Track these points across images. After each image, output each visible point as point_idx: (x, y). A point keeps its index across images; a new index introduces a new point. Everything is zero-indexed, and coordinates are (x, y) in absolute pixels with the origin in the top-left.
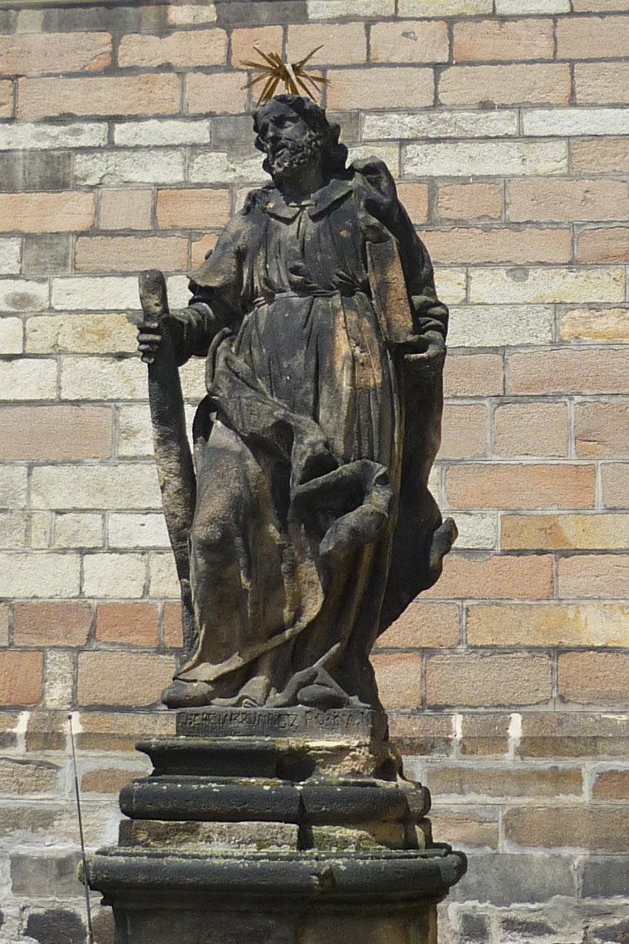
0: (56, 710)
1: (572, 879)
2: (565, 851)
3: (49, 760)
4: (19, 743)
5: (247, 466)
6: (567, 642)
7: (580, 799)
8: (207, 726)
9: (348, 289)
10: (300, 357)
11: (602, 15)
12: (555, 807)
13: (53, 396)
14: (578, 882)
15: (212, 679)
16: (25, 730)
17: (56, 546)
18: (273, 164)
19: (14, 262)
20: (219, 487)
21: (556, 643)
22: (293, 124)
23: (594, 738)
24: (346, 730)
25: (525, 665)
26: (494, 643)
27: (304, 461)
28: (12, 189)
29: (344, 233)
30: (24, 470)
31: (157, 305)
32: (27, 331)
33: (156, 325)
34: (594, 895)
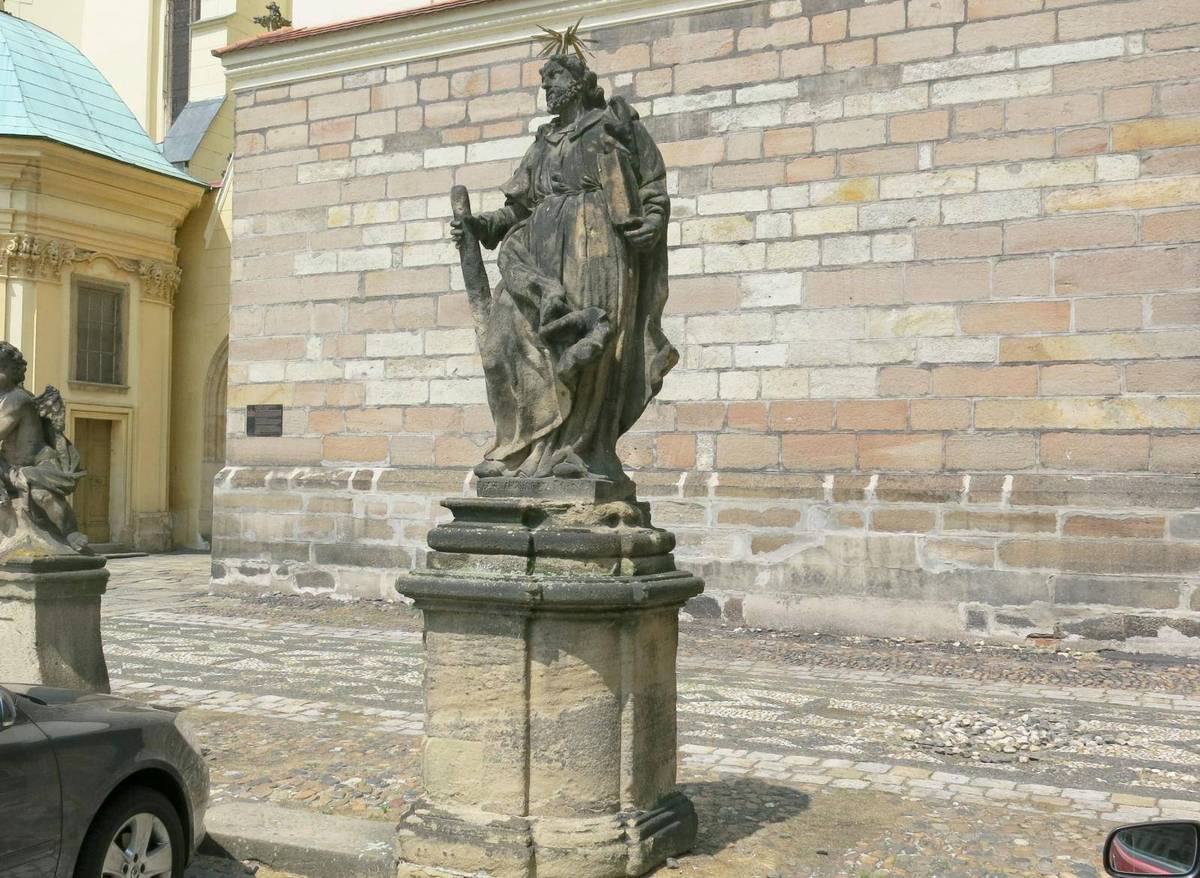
2: (1043, 571)
6: (1047, 426)
13: (700, 271)
14: (1052, 592)
21: (1039, 426)
23: (1065, 493)
28: (673, 140)
34: (1063, 602)
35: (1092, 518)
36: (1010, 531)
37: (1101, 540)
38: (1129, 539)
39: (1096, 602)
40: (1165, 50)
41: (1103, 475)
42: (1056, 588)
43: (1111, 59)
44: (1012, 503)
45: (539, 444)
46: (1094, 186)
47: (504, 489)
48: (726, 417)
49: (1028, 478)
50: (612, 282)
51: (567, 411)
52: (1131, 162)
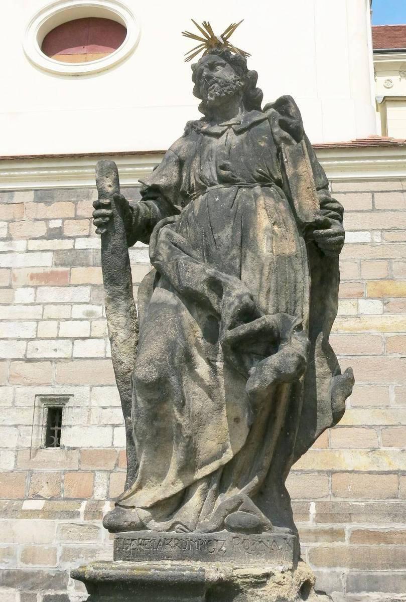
0: (99, 501)
1: (341, 583)
2: (338, 570)
3: (94, 524)
4: (81, 516)
5: (182, 316)
6: (336, 468)
7: (344, 544)
8: (141, 550)
9: (264, 181)
10: (228, 230)
11: (345, 193)
12: (332, 547)
13: (103, 355)
14: (344, 585)
15: (148, 506)
16: (84, 510)
17: (102, 424)
18: (207, 96)
19: (87, 297)
20: (157, 333)
21: (330, 469)
22: (221, 68)
23: (350, 514)
24: (271, 553)
25: (316, 479)
26: (302, 469)
27: (232, 310)
28: (88, 266)
29: (262, 144)
30: (88, 389)
31: (110, 186)
32: (92, 327)
33: (108, 201)
34: (352, 591)
35: (368, 531)
36: (316, 541)
37: (374, 546)
38: (390, 545)
39: (373, 590)
40: (393, 242)
41: (371, 501)
42: (347, 582)
43: (364, 244)
44: (317, 521)
45: (202, 486)
46: (358, 317)
47: (155, 550)
48: (118, 459)
49: (325, 504)
50: (300, 286)
51: (240, 443)
52: (378, 304)
